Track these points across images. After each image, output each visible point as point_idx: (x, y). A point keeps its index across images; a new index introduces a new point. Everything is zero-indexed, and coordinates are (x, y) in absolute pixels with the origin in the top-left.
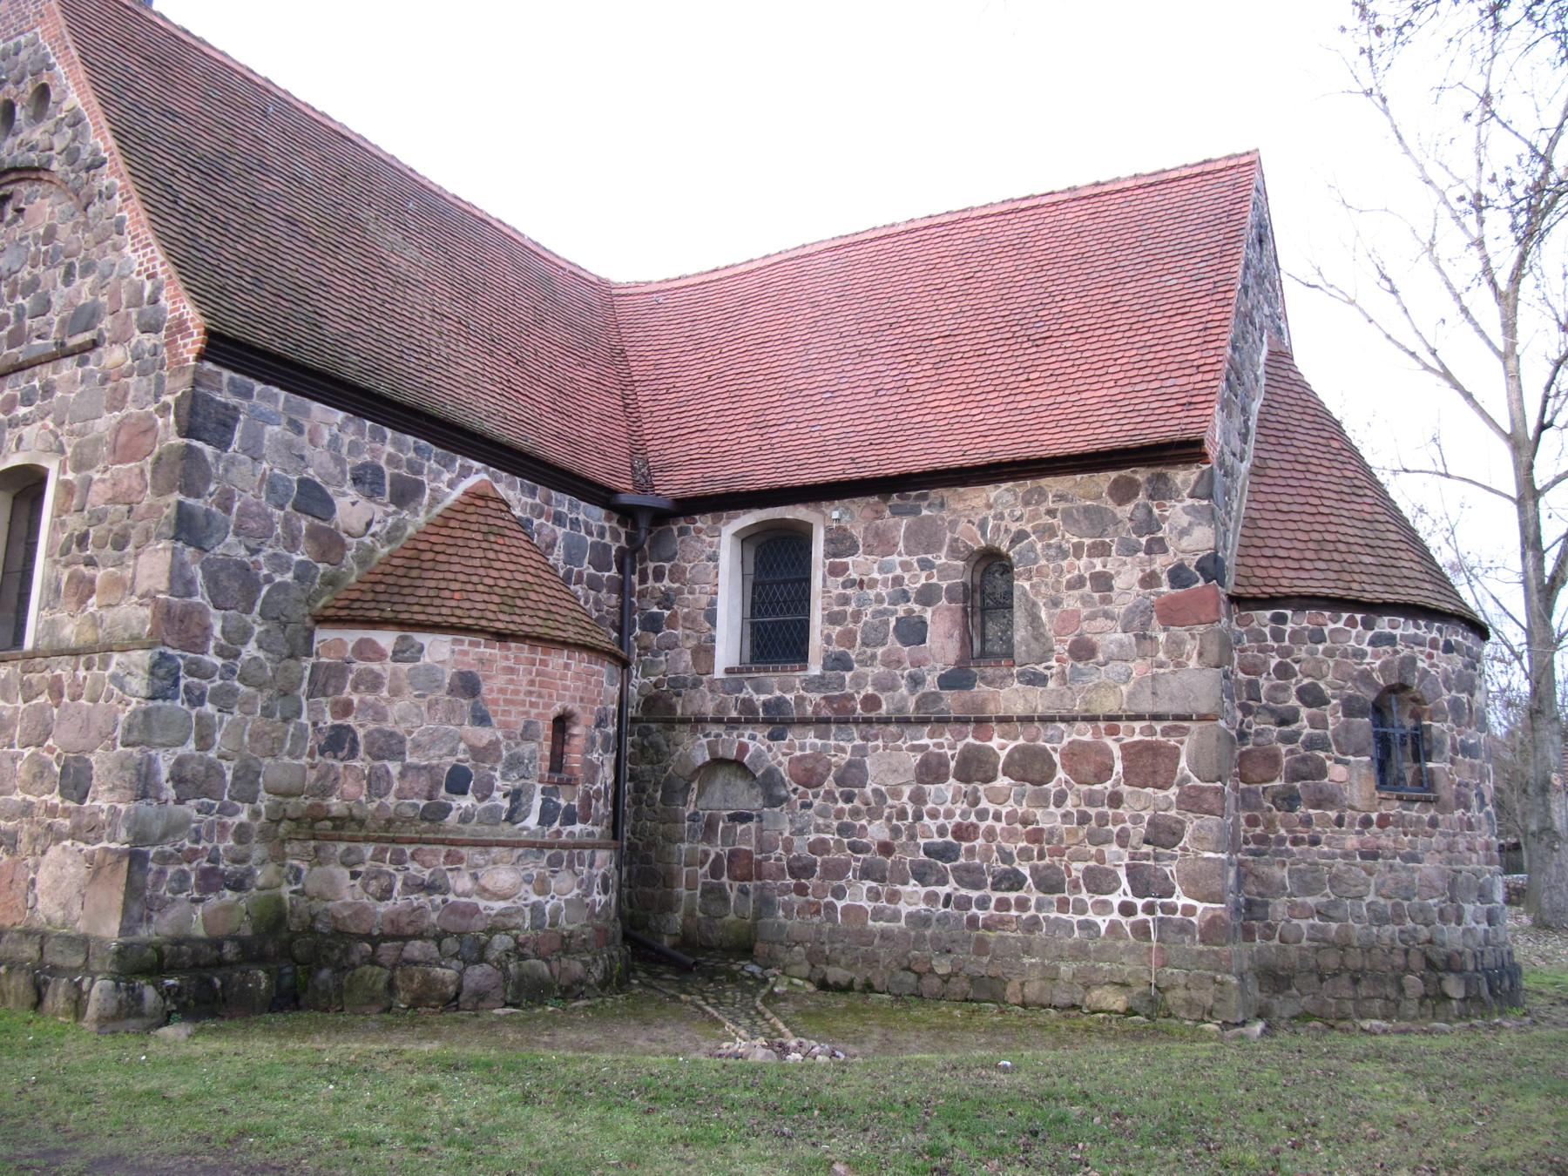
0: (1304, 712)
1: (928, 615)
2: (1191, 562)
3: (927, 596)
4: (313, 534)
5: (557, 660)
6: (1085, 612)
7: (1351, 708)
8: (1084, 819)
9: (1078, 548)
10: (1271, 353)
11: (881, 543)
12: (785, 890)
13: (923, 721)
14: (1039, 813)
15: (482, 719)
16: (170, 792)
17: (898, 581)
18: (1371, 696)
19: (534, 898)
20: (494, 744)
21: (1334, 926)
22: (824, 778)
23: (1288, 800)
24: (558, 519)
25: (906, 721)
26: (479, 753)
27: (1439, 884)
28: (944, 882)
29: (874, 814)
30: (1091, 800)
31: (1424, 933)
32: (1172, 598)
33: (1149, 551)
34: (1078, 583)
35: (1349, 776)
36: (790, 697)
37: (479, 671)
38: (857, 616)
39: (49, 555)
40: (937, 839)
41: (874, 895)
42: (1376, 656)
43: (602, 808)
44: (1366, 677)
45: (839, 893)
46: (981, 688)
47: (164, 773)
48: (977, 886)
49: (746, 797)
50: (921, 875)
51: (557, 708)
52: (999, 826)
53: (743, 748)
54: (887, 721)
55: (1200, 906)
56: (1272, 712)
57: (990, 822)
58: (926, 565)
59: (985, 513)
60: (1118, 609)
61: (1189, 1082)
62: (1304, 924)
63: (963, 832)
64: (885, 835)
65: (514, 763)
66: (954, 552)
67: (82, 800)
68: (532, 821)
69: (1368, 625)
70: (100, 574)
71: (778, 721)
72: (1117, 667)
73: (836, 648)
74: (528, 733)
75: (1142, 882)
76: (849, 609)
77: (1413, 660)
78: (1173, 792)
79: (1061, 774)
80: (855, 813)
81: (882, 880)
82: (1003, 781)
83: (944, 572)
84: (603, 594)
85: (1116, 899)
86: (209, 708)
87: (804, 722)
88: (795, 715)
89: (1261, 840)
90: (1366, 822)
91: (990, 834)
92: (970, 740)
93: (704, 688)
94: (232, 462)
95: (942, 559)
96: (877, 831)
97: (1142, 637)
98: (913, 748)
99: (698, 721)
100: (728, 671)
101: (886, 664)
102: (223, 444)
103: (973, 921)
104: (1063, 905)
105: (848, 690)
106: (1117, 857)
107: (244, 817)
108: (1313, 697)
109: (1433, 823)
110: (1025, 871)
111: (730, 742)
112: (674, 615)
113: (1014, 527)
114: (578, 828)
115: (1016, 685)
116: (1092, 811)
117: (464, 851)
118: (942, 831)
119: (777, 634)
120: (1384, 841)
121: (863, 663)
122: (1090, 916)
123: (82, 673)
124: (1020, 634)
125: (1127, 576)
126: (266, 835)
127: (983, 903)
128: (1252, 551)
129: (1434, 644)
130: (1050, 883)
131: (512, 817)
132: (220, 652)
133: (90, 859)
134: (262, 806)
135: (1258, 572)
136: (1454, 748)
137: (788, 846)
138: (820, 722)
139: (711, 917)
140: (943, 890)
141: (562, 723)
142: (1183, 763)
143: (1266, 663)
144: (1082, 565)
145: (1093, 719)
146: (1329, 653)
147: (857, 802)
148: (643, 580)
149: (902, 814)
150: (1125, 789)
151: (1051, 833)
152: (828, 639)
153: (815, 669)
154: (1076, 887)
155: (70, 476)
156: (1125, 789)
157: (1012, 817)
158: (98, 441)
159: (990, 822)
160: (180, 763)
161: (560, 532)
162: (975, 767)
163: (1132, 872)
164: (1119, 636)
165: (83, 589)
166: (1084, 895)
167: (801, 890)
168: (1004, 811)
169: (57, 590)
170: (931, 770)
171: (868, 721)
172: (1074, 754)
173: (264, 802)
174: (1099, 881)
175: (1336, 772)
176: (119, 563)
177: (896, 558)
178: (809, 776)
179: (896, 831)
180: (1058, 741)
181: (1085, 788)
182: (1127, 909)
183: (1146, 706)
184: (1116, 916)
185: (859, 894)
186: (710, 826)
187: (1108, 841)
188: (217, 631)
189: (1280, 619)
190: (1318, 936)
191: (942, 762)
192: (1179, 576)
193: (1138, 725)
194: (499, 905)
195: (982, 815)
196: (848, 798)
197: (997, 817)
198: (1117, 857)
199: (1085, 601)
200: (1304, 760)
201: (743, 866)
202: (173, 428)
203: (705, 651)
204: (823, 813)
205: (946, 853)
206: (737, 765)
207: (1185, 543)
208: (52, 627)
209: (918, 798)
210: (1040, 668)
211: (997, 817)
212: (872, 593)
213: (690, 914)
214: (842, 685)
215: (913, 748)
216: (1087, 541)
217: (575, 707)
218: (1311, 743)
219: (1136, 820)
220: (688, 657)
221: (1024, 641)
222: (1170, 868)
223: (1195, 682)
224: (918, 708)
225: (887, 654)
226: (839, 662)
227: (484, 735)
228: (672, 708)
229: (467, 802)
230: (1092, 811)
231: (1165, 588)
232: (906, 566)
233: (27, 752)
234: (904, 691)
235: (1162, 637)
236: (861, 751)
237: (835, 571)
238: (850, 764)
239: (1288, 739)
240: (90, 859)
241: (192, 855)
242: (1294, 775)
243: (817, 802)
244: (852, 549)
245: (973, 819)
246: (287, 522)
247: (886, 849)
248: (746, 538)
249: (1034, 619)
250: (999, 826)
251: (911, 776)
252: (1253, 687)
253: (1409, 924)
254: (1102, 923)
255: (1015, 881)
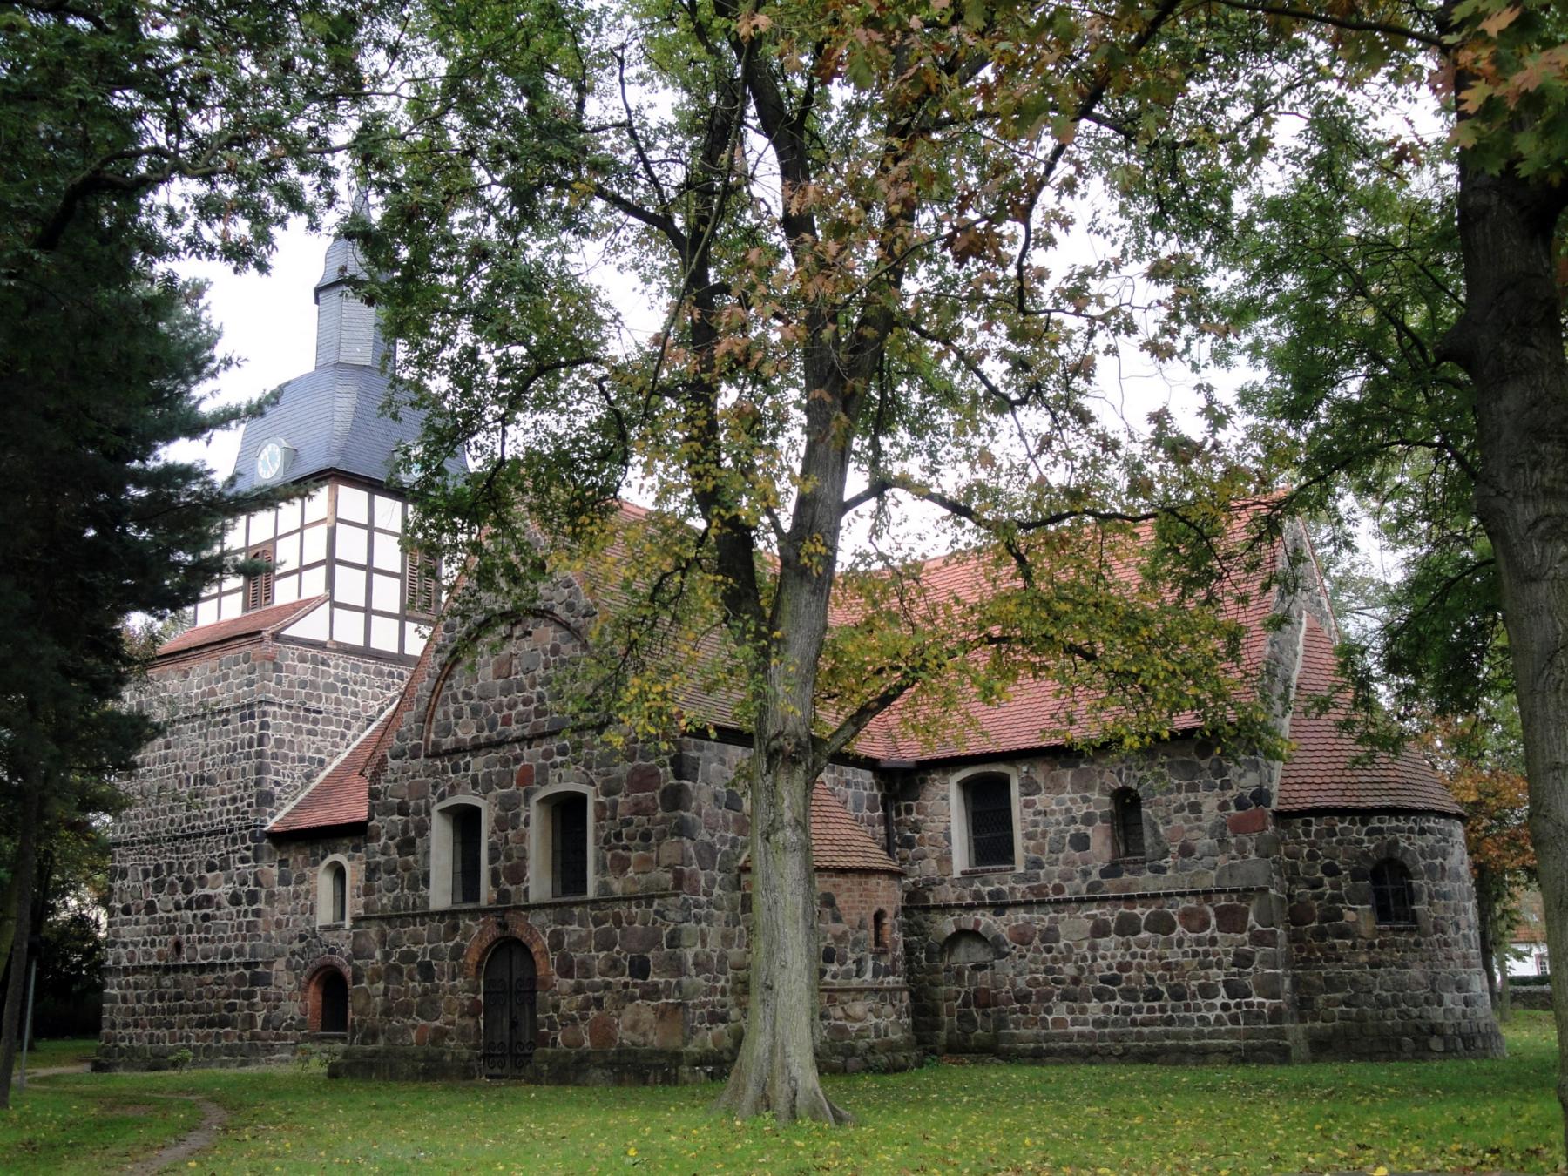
0: (1326, 880)
1: (1090, 831)
2: (1248, 793)
3: (1088, 819)
4: (736, 820)
5: (873, 881)
6: (1186, 827)
7: (1356, 875)
8: (1195, 954)
9: (1179, 787)
10: (1309, 629)
11: (1056, 786)
12: (1014, 1012)
13: (1092, 900)
14: (1168, 952)
15: (837, 919)
16: (693, 972)
17: (1068, 810)
18: (1370, 866)
19: (874, 1020)
20: (845, 933)
21: (1355, 1010)
22: (1032, 939)
23: (1321, 934)
24: (848, 784)
25: (1081, 901)
26: (840, 938)
27: (1423, 981)
28: (1113, 999)
29: (1066, 960)
30: (1199, 942)
31: (1415, 1012)
32: (1239, 818)
33: (1222, 788)
34: (1180, 809)
35: (1358, 916)
36: (1005, 888)
37: (832, 891)
38: (1044, 834)
39: (596, 843)
40: (1108, 973)
41: (1071, 1011)
42: (1370, 842)
43: (900, 966)
44: (1365, 854)
45: (1049, 1011)
46: (1126, 877)
47: (690, 961)
48: (1135, 1000)
49: (980, 954)
50: (1100, 995)
51: (875, 909)
52: (1145, 962)
53: (977, 923)
54: (1069, 901)
55: (1267, 1002)
56: (1306, 881)
57: (1139, 960)
58: (1086, 800)
59: (1120, 766)
60: (1206, 825)
61: (528, 483)
62: (1336, 1010)
63: (1124, 967)
64: (1074, 972)
65: (856, 943)
66: (1103, 791)
67: (645, 978)
68: (868, 976)
69: (1364, 824)
70: (633, 855)
71: (999, 906)
72: (1208, 860)
73: (1033, 855)
74: (861, 927)
75: (1234, 990)
76: (1039, 830)
77: (1396, 842)
78: (1246, 935)
79: (1179, 928)
80: (1054, 960)
81: (1075, 1000)
82: (1144, 935)
83: (1098, 804)
84: (877, 828)
85: (1218, 1002)
86: (704, 925)
87: (1016, 904)
88: (1010, 900)
89: (1306, 960)
90: (1371, 946)
91: (1140, 966)
92: (1122, 909)
93: (947, 885)
94: (700, 788)
95: (1095, 796)
96: (1069, 970)
97: (1223, 842)
98: (1088, 917)
99: (945, 908)
100: (963, 873)
101: (1066, 863)
102: (695, 780)
103: (1134, 1023)
104: (1187, 1007)
105: (1043, 882)
106: (1217, 976)
107: (722, 983)
108: (1331, 870)
109: (1417, 944)
110: (1163, 989)
111: (968, 920)
112: (922, 837)
113: (1139, 774)
114: (891, 978)
115: (1148, 874)
116: (1200, 949)
117: (837, 995)
118: (1110, 968)
119: (992, 840)
120: (1384, 957)
121: (1051, 864)
122: (1204, 1013)
123: (634, 910)
124: (1148, 841)
125: (1210, 803)
126: (733, 991)
127: (1139, 1010)
128: (1291, 780)
129: (1411, 830)
130: (1178, 994)
131: (859, 974)
132: (705, 894)
133: (655, 1009)
134: (729, 976)
135: (1293, 794)
136: (1430, 896)
137: (1013, 985)
138: (1027, 905)
139: (965, 1033)
140: (1113, 1004)
141: (879, 917)
142: (1251, 917)
143: (1301, 851)
144: (1182, 798)
145: (1195, 894)
146: (1340, 843)
147: (1055, 953)
148: (899, 814)
149: (1084, 959)
150: (1217, 934)
151: (1177, 964)
152: (1027, 849)
153: (1020, 868)
154: (1194, 996)
155: (602, 799)
156: (1217, 934)
157: (1152, 955)
158: (619, 780)
159: (1139, 960)
160: (696, 955)
161: (850, 791)
162: (1127, 927)
163: (1226, 983)
164: (1208, 840)
165: (621, 866)
166: (1199, 1000)
167: (1024, 1011)
168: (1147, 952)
169: (604, 865)
170: (1100, 930)
171: (1057, 902)
172: (1187, 915)
173: (730, 974)
174: (1207, 991)
175: (1350, 916)
176: (647, 849)
177: (1066, 796)
178: (1023, 938)
179: (1081, 969)
180: (1174, 910)
181: (1194, 935)
182: (1225, 1007)
183: (1228, 886)
184: (1219, 1012)
185: (1061, 1010)
186: (959, 974)
187: (1210, 967)
188: (703, 883)
189: (1309, 823)
190: (1344, 1017)
191: (1106, 922)
192: (1240, 803)
193: (1223, 897)
194: (857, 1026)
195: (1134, 956)
196: (1049, 950)
197: (1143, 957)
198: (1217, 976)
199: (1186, 820)
200: (1329, 909)
201: (983, 999)
202: (670, 775)
203: (945, 859)
204: (1033, 961)
205: (1113, 980)
206: (974, 935)
207: (1243, 782)
208: (604, 887)
209: (1093, 948)
210: (1162, 863)
211: (1143, 957)
212: (1052, 819)
213: (951, 1032)
214: (1038, 879)
215: (1088, 917)
216: (1184, 783)
217: (884, 907)
218: (1333, 899)
219: (1227, 953)
220: (934, 863)
221: (1151, 845)
222: (1248, 981)
223: (1254, 868)
224: (1088, 891)
225: (1066, 858)
226: (1036, 864)
227: (841, 928)
228: (927, 899)
229: (834, 967)
230: (1200, 949)
231: (1233, 811)
232: (1073, 801)
233: (602, 955)
234: (1078, 881)
235: (1233, 841)
236: (1054, 921)
237: (1027, 805)
238: (1049, 929)
239: (1319, 897)
240: (655, 1009)
241: (704, 1005)
242: (1323, 919)
243: (1029, 955)
244: (1037, 791)
245: (1128, 958)
246: (724, 817)
247: (1076, 981)
248: (964, 785)
249: (1156, 832)
250: (1145, 962)
251: (1087, 934)
252: (1294, 866)
253: (1404, 1006)
254: (1212, 1017)
255: (1157, 995)
